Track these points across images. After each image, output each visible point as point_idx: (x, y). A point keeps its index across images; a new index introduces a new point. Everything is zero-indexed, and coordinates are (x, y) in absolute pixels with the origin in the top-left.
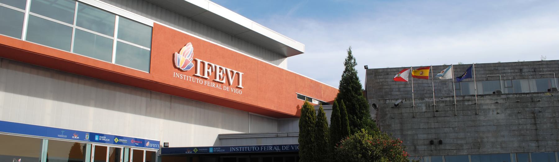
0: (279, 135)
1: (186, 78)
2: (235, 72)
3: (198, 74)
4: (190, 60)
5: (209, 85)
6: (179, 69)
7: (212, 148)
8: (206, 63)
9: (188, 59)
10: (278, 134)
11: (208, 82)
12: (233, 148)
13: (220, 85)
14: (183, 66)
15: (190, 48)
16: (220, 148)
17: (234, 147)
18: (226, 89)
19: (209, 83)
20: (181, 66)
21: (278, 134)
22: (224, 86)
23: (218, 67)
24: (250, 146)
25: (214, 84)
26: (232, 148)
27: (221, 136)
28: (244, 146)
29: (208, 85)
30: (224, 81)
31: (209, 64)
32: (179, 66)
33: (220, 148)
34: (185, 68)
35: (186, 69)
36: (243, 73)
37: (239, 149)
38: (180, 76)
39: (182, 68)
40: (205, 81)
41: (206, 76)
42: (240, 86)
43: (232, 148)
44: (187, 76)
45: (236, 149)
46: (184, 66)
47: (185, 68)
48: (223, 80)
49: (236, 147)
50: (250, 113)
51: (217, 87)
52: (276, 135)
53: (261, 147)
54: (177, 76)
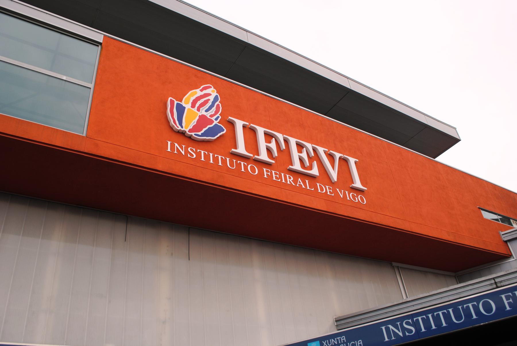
0: (501, 282)
1: (207, 157)
2: (338, 155)
3: (241, 149)
4: (213, 118)
5: (276, 177)
6: (183, 133)
7: (318, 342)
8: (261, 131)
9: (208, 115)
10: (497, 280)
11: (273, 172)
12: (391, 327)
13: (307, 181)
14: (194, 126)
15: (209, 95)
16: (343, 338)
17: (393, 322)
18: (324, 191)
19: (276, 174)
20: (188, 123)
21: (497, 280)
22: (318, 184)
23: (293, 141)
24: (454, 306)
25: (290, 178)
26: (388, 329)
27: (343, 322)
28: (432, 311)
29: (274, 179)
30: (315, 171)
31: (266, 134)
32: (182, 127)
33: (343, 338)
34: (200, 133)
35: (203, 135)
36: (357, 160)
37: (416, 324)
38: (187, 152)
39: (190, 131)
40: (265, 169)
41: (264, 156)
42: (358, 184)
43: (388, 329)
44: (211, 154)
45: (404, 329)
46: (195, 129)
47: (200, 133)
48: (311, 168)
49: (402, 319)
50: (394, 264)
51: (300, 185)
52: (491, 284)
53: (503, 296)
54: (178, 150)
